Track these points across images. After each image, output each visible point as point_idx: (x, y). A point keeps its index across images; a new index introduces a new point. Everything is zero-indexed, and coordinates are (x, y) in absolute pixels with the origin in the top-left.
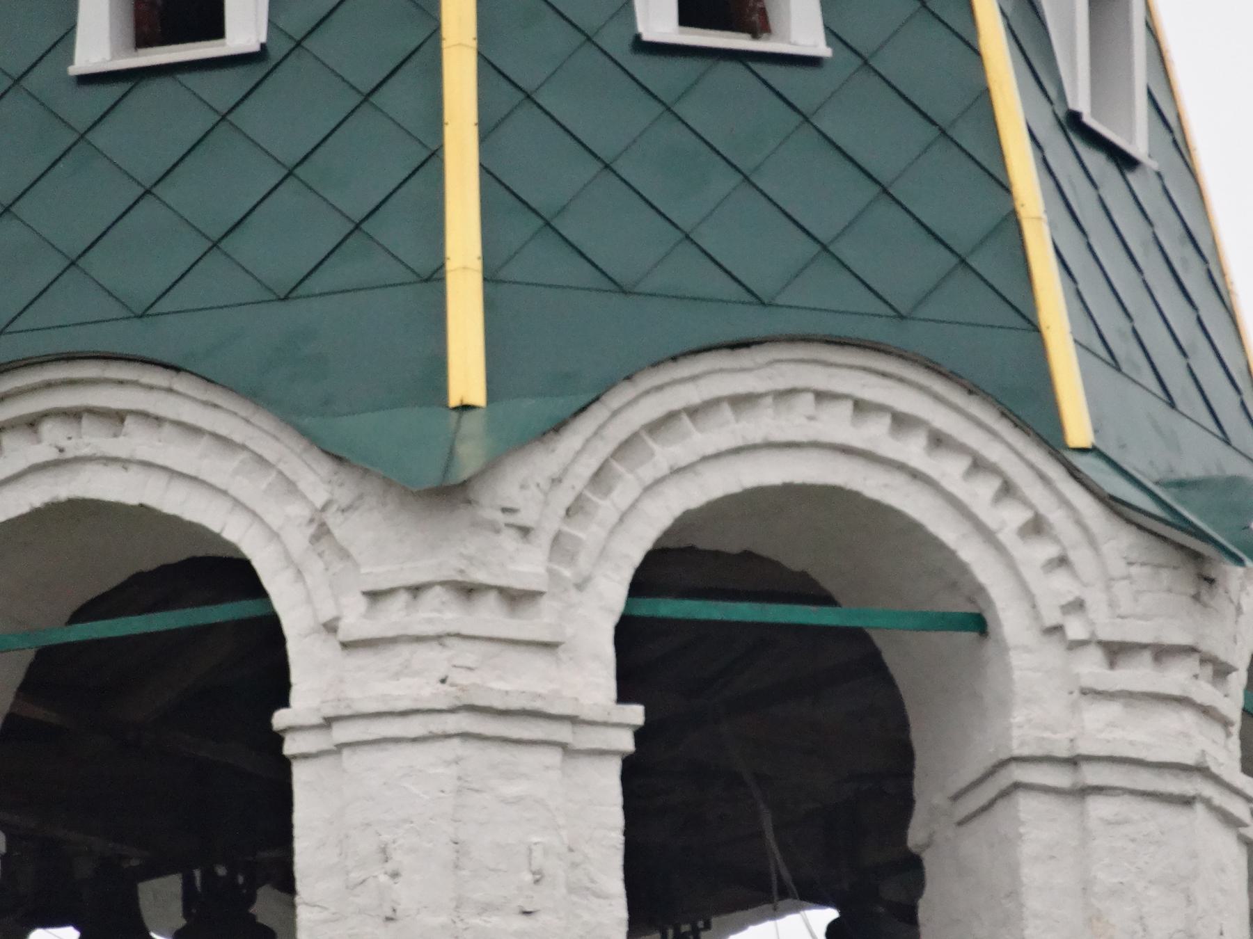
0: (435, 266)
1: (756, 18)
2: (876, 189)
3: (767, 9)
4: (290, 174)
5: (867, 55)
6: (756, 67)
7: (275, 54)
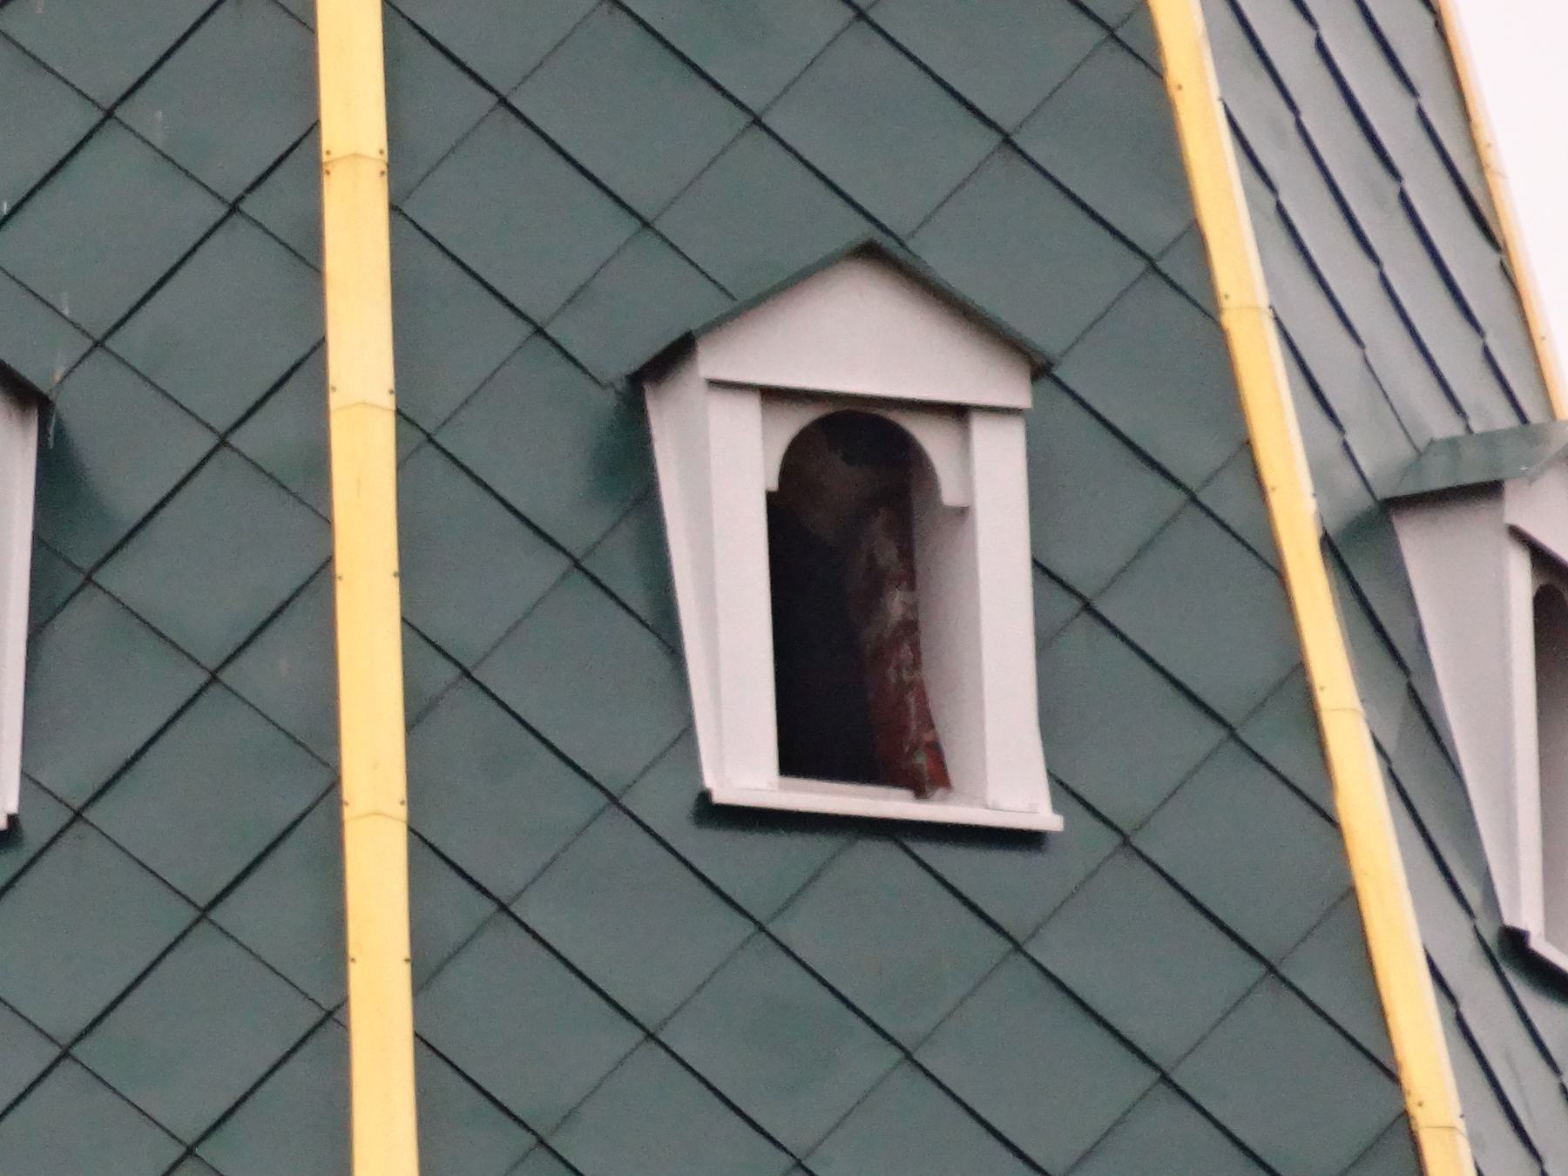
0: (313, 121)
1: (921, 760)
2: (1149, 1076)
3: (946, 749)
4: (65, 1054)
5: (1126, 828)
6: (926, 851)
7: (35, 835)
